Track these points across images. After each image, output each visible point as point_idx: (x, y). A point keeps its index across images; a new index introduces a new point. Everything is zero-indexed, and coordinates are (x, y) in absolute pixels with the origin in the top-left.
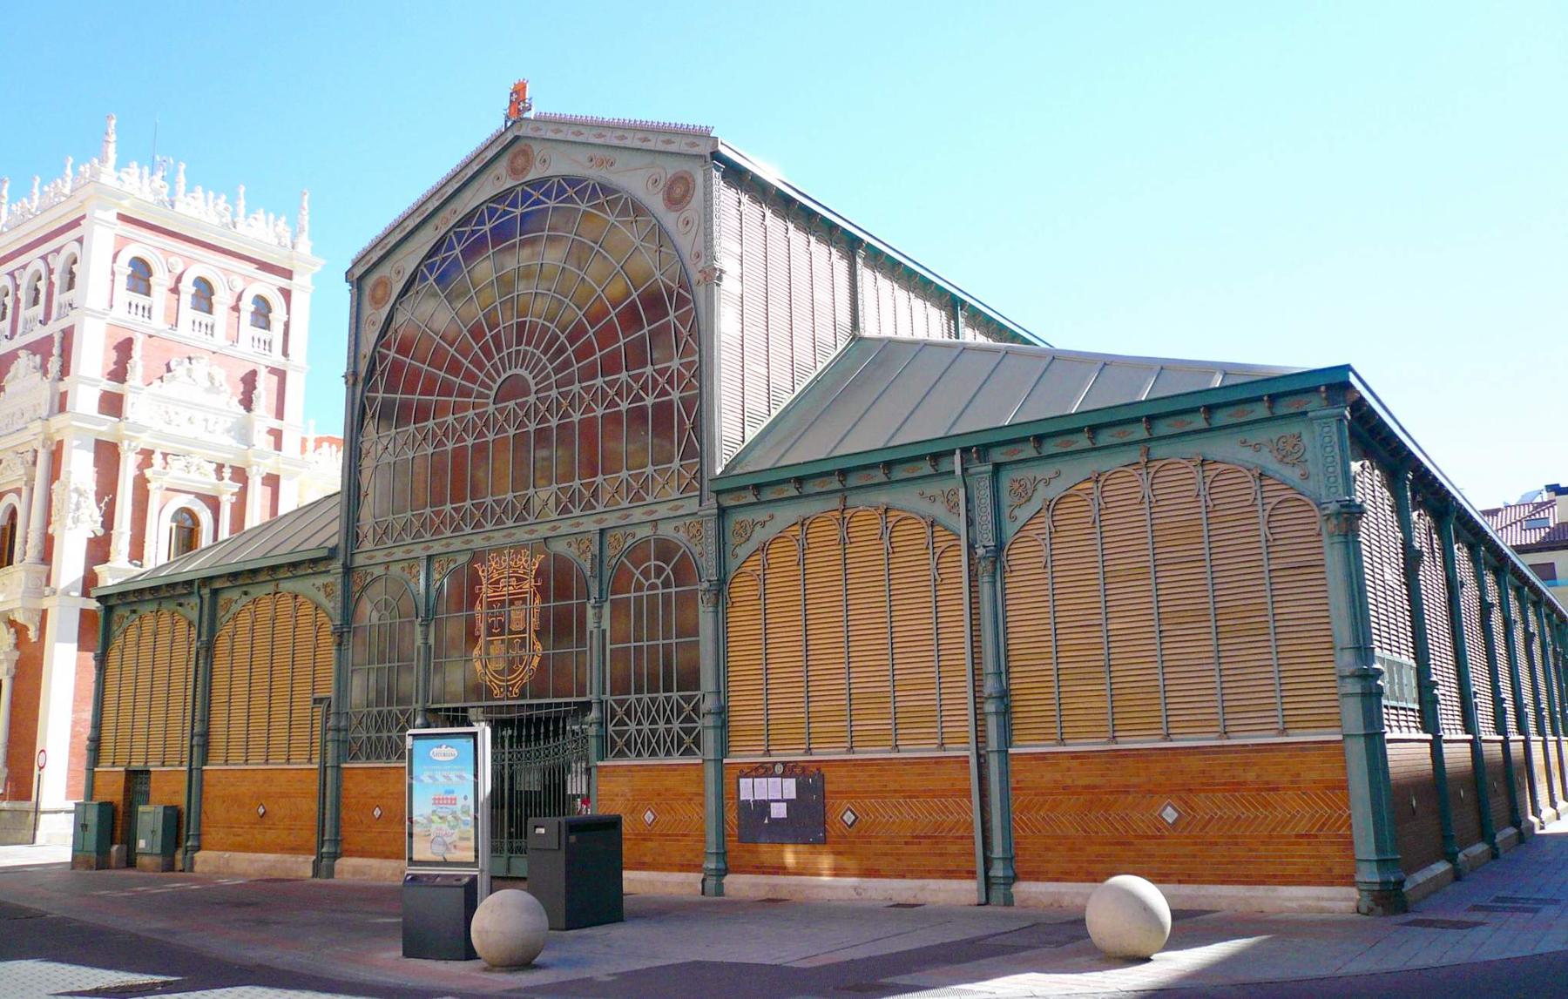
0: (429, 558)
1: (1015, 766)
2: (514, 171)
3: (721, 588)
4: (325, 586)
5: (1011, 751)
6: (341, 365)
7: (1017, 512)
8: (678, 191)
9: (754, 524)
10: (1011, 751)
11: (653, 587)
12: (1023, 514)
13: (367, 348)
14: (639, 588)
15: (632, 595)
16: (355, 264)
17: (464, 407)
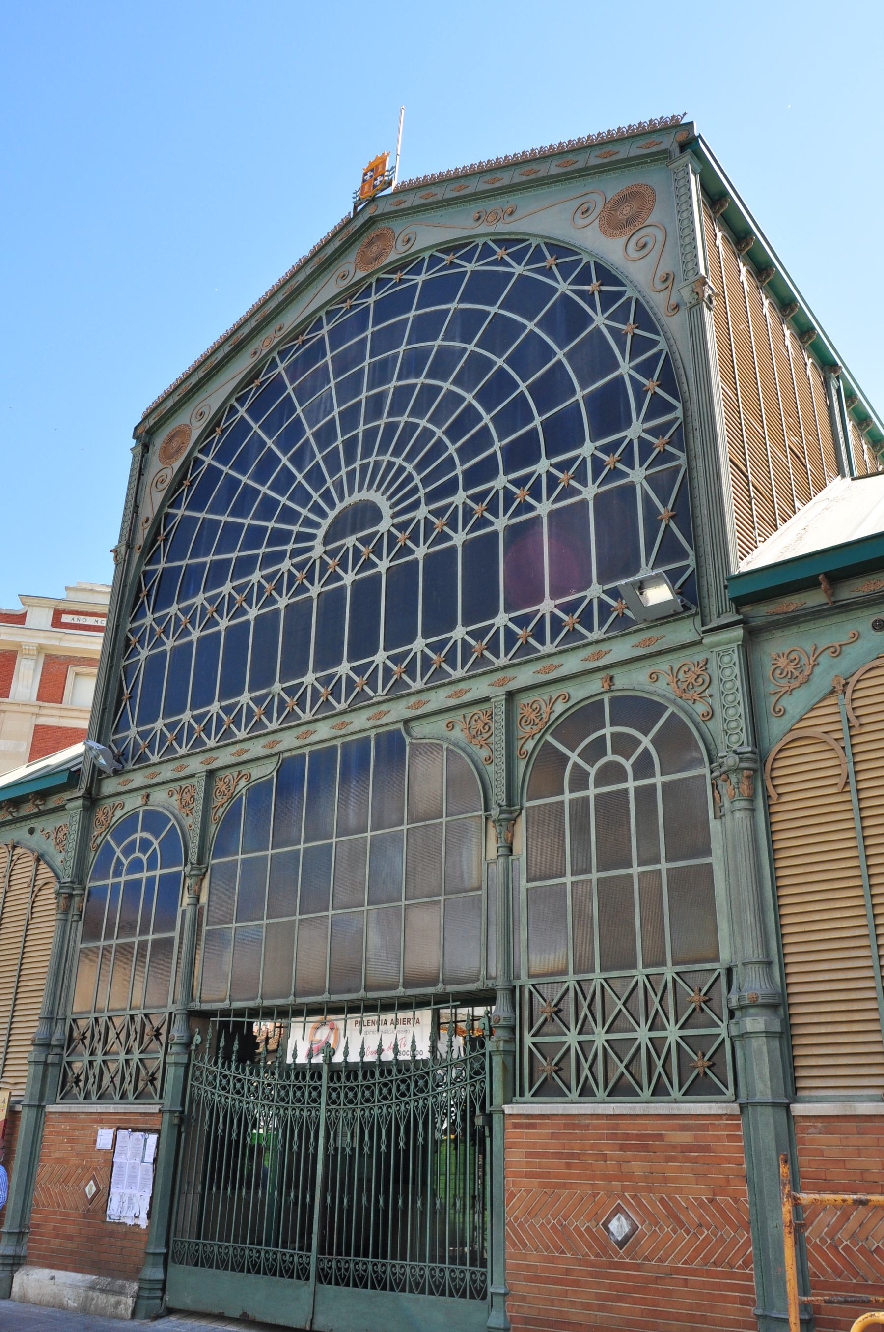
0: (511, 695)
1: (814, 1138)
2: (365, 261)
3: (758, 763)
4: (57, 831)
5: (798, 1109)
6: (112, 535)
7: (785, 702)
8: (626, 211)
9: (817, 653)
10: (798, 1109)
11: (612, 773)
12: (795, 704)
13: (149, 509)
14: (580, 781)
15: (567, 796)
16: (146, 418)
17: (279, 557)
